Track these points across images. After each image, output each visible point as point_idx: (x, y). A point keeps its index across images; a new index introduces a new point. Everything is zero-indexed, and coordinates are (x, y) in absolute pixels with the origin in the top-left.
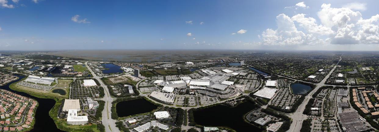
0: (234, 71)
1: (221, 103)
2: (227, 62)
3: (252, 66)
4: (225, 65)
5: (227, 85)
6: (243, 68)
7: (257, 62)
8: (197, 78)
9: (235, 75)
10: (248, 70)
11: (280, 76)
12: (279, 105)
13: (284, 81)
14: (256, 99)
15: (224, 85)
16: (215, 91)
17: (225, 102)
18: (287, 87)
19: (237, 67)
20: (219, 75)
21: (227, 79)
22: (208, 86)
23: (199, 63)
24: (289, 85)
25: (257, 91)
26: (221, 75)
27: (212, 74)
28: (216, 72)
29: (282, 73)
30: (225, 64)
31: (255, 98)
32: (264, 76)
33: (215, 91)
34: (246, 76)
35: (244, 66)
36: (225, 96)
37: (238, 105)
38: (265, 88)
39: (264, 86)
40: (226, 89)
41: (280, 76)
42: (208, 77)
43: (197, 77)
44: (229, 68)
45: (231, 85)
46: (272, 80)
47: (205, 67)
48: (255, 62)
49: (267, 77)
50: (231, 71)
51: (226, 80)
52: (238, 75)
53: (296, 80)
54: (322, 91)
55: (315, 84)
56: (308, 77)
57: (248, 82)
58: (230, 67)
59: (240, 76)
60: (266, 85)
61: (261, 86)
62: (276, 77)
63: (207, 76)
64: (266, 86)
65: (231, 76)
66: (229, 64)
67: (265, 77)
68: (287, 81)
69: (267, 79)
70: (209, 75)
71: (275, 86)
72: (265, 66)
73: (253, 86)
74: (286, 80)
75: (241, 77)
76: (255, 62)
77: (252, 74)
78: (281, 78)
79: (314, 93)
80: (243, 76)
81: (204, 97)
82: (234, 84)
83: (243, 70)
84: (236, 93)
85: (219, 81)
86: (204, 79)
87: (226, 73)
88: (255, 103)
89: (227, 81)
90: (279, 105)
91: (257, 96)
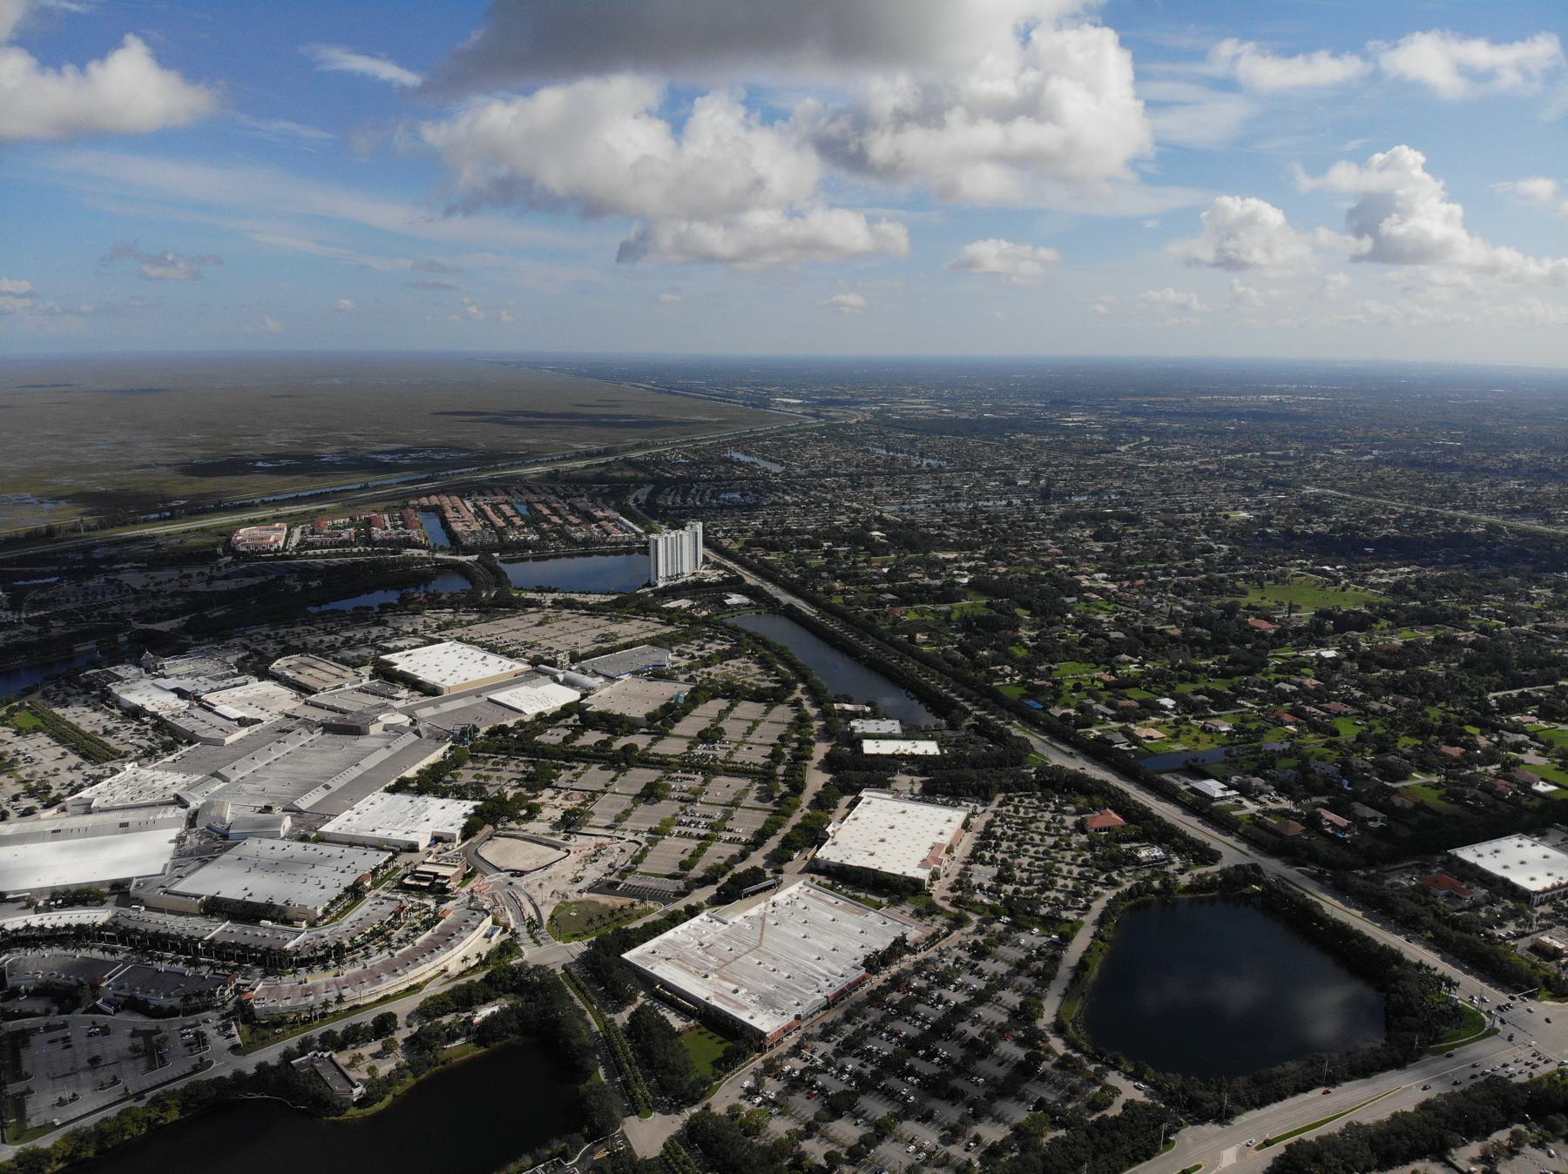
0: (540, 666)
1: (239, 1075)
2: (484, 550)
3: (786, 598)
4: (459, 585)
5: (379, 846)
6: (670, 617)
7: (874, 548)
8: (27, 803)
9: (531, 711)
10: (714, 647)
11: (1060, 759)
12: (807, 1145)
13: (1080, 827)
14: (622, 1018)
15: (352, 843)
16: (218, 929)
17: (287, 1056)
18: (1049, 922)
19: (594, 610)
20: (328, 728)
21: (410, 773)
22: (146, 880)
23: (97, 582)
24: (1098, 906)
25: (692, 912)
26: (347, 727)
27: (243, 722)
28: (303, 689)
29: (1124, 716)
30: (460, 569)
31: (622, 1001)
32: (870, 726)
33: (218, 929)
34: (668, 715)
35: (695, 588)
36: (318, 978)
37: (412, 1091)
38: (795, 890)
39: (799, 859)
40: (355, 893)
41: (1060, 759)
42: (175, 767)
43: (31, 793)
44: (483, 630)
45: (437, 839)
46: (928, 794)
47: (163, 626)
48: (859, 539)
49: (887, 748)
50: (497, 667)
51: (400, 787)
52: (567, 710)
53: (1232, 852)
54: (1475, 1149)
55: (1470, 989)
56: (1467, 854)
57: (650, 794)
58: (515, 606)
59: (577, 731)
60: (826, 853)
61: (757, 859)
62: (999, 763)
63: (169, 748)
64: (815, 868)
65: (467, 733)
66: (513, 571)
67: (869, 747)
68: (1116, 837)
69: (879, 773)
70: (191, 739)
71: (923, 874)
72: (949, 593)
73: (672, 850)
74: (1115, 819)
75: (591, 738)
76: (859, 539)
77: (733, 693)
78: (1058, 785)
79: (1334, 1127)
80: (613, 723)
81: (80, 1021)
82: (468, 832)
83: (654, 642)
84: (447, 939)
85: (304, 803)
86: (123, 796)
87: (432, 691)
88: (588, 1073)
89: (402, 799)
90: (807, 1145)
91: (648, 981)
